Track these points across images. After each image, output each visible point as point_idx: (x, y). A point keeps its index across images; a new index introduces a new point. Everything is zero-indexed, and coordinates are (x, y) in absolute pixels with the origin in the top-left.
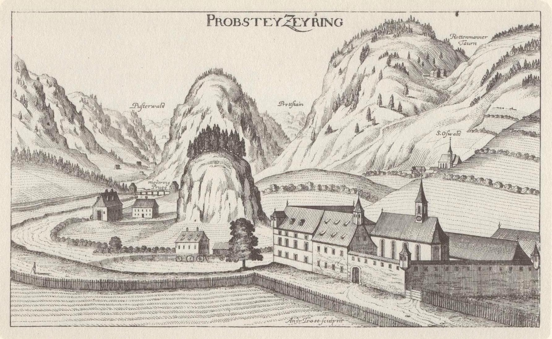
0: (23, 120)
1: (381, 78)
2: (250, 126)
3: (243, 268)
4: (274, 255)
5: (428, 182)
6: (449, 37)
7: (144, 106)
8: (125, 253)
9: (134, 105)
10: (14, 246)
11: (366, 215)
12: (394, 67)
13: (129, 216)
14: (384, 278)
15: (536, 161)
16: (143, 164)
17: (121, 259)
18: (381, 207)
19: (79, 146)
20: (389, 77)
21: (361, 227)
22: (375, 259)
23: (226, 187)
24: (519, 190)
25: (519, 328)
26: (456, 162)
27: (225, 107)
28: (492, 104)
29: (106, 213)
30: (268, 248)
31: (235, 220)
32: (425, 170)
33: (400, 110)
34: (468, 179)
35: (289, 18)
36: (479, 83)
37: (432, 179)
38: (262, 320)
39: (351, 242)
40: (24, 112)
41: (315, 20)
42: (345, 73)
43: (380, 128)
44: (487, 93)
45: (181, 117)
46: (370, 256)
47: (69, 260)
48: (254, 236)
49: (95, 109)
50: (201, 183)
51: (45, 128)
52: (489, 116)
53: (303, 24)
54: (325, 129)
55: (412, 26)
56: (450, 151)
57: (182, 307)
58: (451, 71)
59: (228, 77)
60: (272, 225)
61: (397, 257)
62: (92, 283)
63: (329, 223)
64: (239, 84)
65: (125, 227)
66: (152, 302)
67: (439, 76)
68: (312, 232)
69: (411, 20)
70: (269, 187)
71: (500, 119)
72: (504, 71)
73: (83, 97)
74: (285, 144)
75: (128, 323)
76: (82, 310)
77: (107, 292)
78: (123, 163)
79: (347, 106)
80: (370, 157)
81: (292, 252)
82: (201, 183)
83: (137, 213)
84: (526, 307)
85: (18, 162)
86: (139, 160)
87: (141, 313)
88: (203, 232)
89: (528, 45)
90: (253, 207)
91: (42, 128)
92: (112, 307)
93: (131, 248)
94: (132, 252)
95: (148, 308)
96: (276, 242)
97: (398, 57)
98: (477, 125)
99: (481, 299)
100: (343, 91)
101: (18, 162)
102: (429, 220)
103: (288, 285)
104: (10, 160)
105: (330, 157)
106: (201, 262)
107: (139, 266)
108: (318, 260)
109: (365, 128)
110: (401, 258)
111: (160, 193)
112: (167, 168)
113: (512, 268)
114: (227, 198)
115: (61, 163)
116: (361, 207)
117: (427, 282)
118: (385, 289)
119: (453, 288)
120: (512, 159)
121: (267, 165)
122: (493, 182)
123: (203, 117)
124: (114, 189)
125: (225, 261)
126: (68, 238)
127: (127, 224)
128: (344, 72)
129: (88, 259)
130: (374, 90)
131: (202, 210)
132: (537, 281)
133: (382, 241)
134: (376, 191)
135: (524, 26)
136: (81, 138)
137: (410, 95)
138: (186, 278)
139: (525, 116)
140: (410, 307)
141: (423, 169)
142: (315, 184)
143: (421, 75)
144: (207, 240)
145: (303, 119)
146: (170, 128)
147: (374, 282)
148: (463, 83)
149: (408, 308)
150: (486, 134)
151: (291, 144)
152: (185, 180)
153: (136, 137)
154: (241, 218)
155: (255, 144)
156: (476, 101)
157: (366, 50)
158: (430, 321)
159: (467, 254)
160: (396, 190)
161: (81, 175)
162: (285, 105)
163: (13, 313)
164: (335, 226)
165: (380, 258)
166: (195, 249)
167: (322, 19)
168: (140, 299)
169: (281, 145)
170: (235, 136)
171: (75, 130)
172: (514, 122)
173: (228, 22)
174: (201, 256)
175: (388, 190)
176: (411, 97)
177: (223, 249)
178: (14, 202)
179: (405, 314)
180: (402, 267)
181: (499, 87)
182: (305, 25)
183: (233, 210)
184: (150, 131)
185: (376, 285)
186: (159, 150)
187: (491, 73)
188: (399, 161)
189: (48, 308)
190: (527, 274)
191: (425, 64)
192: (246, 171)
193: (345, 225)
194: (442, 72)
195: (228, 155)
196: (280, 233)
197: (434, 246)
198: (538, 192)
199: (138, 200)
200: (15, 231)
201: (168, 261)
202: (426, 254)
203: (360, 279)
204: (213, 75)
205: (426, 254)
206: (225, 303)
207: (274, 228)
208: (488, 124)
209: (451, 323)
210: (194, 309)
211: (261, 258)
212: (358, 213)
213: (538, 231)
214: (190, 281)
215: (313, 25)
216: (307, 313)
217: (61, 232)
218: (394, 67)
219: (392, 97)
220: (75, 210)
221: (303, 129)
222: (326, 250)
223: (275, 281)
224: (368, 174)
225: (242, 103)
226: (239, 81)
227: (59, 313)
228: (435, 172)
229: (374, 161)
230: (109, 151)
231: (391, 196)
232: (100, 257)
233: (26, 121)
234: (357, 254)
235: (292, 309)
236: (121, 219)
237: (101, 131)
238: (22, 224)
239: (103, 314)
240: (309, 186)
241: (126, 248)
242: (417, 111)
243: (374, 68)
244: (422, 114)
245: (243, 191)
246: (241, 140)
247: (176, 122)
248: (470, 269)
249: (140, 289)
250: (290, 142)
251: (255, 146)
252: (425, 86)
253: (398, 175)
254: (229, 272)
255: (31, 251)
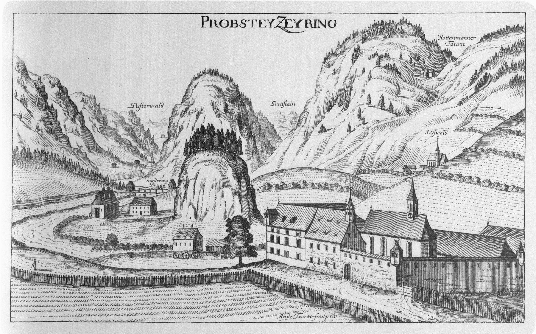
0: (23, 119)
2: (246, 126)
3: (239, 264)
4: (267, 252)
5: (419, 180)
6: (437, 38)
7: (142, 106)
8: (122, 250)
9: (133, 105)
10: (15, 243)
11: (357, 213)
12: (385, 68)
13: (127, 213)
14: (373, 274)
15: (521, 160)
16: (142, 162)
18: (370, 204)
19: (80, 145)
20: (378, 77)
21: (353, 225)
22: (364, 256)
23: (221, 185)
24: (507, 188)
25: (506, 323)
26: (442, 161)
27: (221, 107)
28: (481, 104)
29: (103, 210)
31: (231, 218)
32: (416, 168)
33: (391, 109)
34: (455, 177)
35: (281, 19)
36: (467, 84)
37: (422, 177)
38: (256, 315)
39: (343, 239)
40: (24, 112)
42: (339, 73)
43: (369, 127)
44: (475, 93)
45: (179, 116)
46: (360, 253)
47: (70, 256)
48: (250, 233)
49: (94, 108)
50: (195, 182)
51: (48, 128)
52: (477, 115)
53: (295, 25)
54: (318, 128)
55: (404, 27)
56: (438, 149)
57: (178, 303)
58: (438, 72)
59: (224, 77)
60: (265, 223)
61: (388, 253)
62: (60, 277)
63: (322, 221)
64: (236, 84)
65: (122, 225)
66: (149, 298)
67: (428, 76)
68: (305, 229)
69: (403, 22)
70: (263, 185)
71: (489, 119)
72: (493, 71)
73: (84, 97)
74: (277, 143)
75: (125, 318)
76: (81, 305)
77: (103, 288)
78: (120, 161)
80: (360, 156)
81: (283, 249)
82: (195, 182)
83: (135, 211)
84: (512, 303)
85: (19, 160)
86: (137, 159)
87: (139, 309)
88: (197, 229)
89: (514, 46)
90: (249, 205)
91: (44, 127)
92: (108, 303)
95: (145, 304)
96: (269, 240)
97: (389, 58)
98: (466, 124)
99: (469, 295)
100: (337, 91)
101: (19, 160)
102: (420, 217)
103: (279, 282)
104: (12, 159)
105: (323, 156)
106: (196, 258)
107: (138, 263)
108: (311, 257)
109: (356, 127)
110: (392, 255)
111: (159, 191)
113: (499, 264)
115: (64, 162)
116: (352, 205)
117: (417, 278)
118: (374, 285)
119: (440, 285)
120: (502, 158)
122: (481, 180)
123: (198, 117)
124: (110, 187)
125: (220, 258)
126: (70, 235)
127: (124, 221)
128: (337, 73)
129: (87, 255)
130: (364, 90)
131: (196, 207)
132: (522, 277)
133: (371, 238)
134: (365, 189)
136: (82, 137)
137: (402, 94)
138: (183, 275)
139: (512, 115)
140: (401, 303)
141: (414, 167)
142: (308, 182)
143: (413, 75)
144: (201, 237)
145: (294, 118)
146: (169, 127)
147: (364, 279)
148: (450, 83)
150: (474, 133)
151: (282, 143)
153: (134, 136)
155: (251, 144)
156: (464, 100)
157: (358, 51)
158: (419, 317)
159: (454, 251)
160: (386, 188)
161: (82, 173)
163: (13, 309)
164: (328, 224)
167: (315, 21)
168: (137, 294)
170: (231, 135)
171: (76, 129)
172: (502, 121)
173: (224, 24)
174: (196, 253)
175: (377, 188)
176: (403, 97)
177: (219, 246)
178: (14, 200)
179: (397, 310)
180: (393, 263)
181: (488, 86)
182: (297, 26)
183: (229, 207)
184: (149, 130)
185: (365, 281)
186: (157, 149)
187: (479, 73)
188: (390, 160)
189: (49, 303)
190: (512, 271)
191: (416, 64)
192: (243, 169)
193: (338, 223)
194: (431, 72)
195: (224, 154)
196: (272, 231)
197: (423, 243)
198: (523, 191)
200: (15, 227)
201: (166, 258)
202: (417, 251)
203: (351, 275)
205: (417, 251)
206: (220, 299)
207: (267, 225)
208: (477, 123)
209: (438, 318)
210: (189, 305)
211: (255, 255)
212: (350, 210)
213: (523, 229)
214: (185, 277)
215: (306, 26)
216: (299, 309)
217: (64, 228)
218: (385, 68)
219: (382, 97)
220: (76, 208)
221: (295, 129)
223: (268, 277)
224: (358, 173)
225: (239, 103)
226: (235, 81)
227: (61, 308)
228: (425, 170)
229: (363, 159)
230: (106, 150)
231: (382, 194)
232: (98, 254)
234: (349, 250)
235: (283, 305)
236: (119, 216)
237: (99, 130)
238: (22, 221)
239: (100, 310)
241: (123, 245)
242: (408, 111)
243: (364, 69)
244: (413, 114)
245: (240, 189)
246: (238, 139)
247: (174, 121)
248: (458, 265)
249: (138, 285)
250: (282, 141)
251: (251, 145)
252: (416, 86)
253: (389, 173)
254: (224, 268)
255: (31, 248)
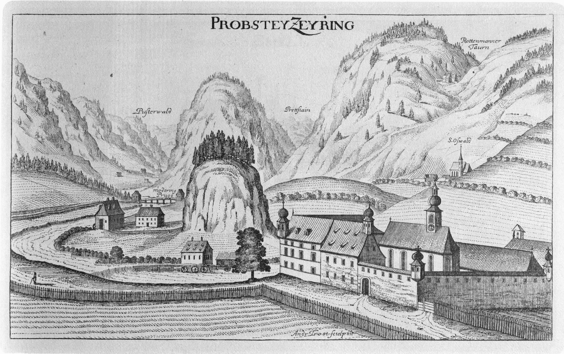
0: (22, 125)
1: (389, 83)
4: (280, 266)
11: (376, 224)
12: (405, 72)
14: (393, 290)
16: (148, 171)
17: (122, 270)
19: (82, 153)
26: (466, 171)
27: (232, 113)
28: (506, 110)
30: (275, 259)
31: (243, 230)
34: (479, 188)
35: (295, 21)
40: (24, 118)
41: (324, 23)
44: (501, 98)
45: (187, 123)
48: (263, 246)
50: (205, 191)
53: (310, 27)
54: (335, 135)
59: (234, 81)
61: (409, 268)
65: (126, 237)
67: (450, 81)
68: (321, 242)
70: (276, 195)
72: (519, 76)
76: (85, 322)
79: (357, 111)
80: (379, 164)
81: (297, 263)
82: (205, 191)
83: (141, 223)
86: (143, 167)
93: (134, 257)
94: (135, 262)
96: (283, 253)
98: (490, 132)
106: (205, 273)
108: (327, 271)
110: (413, 269)
112: (173, 175)
113: (526, 279)
114: (234, 207)
121: (275, 173)
122: (507, 191)
124: (115, 197)
125: (231, 272)
128: (355, 77)
135: (538, 29)
140: (422, 320)
144: (211, 250)
149: (420, 321)
152: (190, 188)
153: (140, 143)
154: (249, 228)
155: (264, 150)
156: (488, 107)
158: (441, 334)
159: (479, 264)
161: (85, 183)
162: (291, 111)
165: (388, 269)
166: (200, 259)
167: (332, 22)
169: (287, 151)
170: (243, 143)
171: (79, 136)
173: (235, 25)
175: (397, 199)
182: (313, 28)
185: (384, 297)
187: (504, 78)
191: (438, 68)
199: (142, 209)
202: (439, 264)
204: (218, 79)
211: (268, 269)
215: (322, 28)
216: (315, 326)
218: (405, 72)
221: (309, 136)
222: (335, 261)
227: (63, 324)
232: (102, 268)
233: (25, 127)
234: (366, 264)
235: (298, 322)
240: (317, 194)
241: (127, 257)
242: (430, 118)
246: (249, 147)
